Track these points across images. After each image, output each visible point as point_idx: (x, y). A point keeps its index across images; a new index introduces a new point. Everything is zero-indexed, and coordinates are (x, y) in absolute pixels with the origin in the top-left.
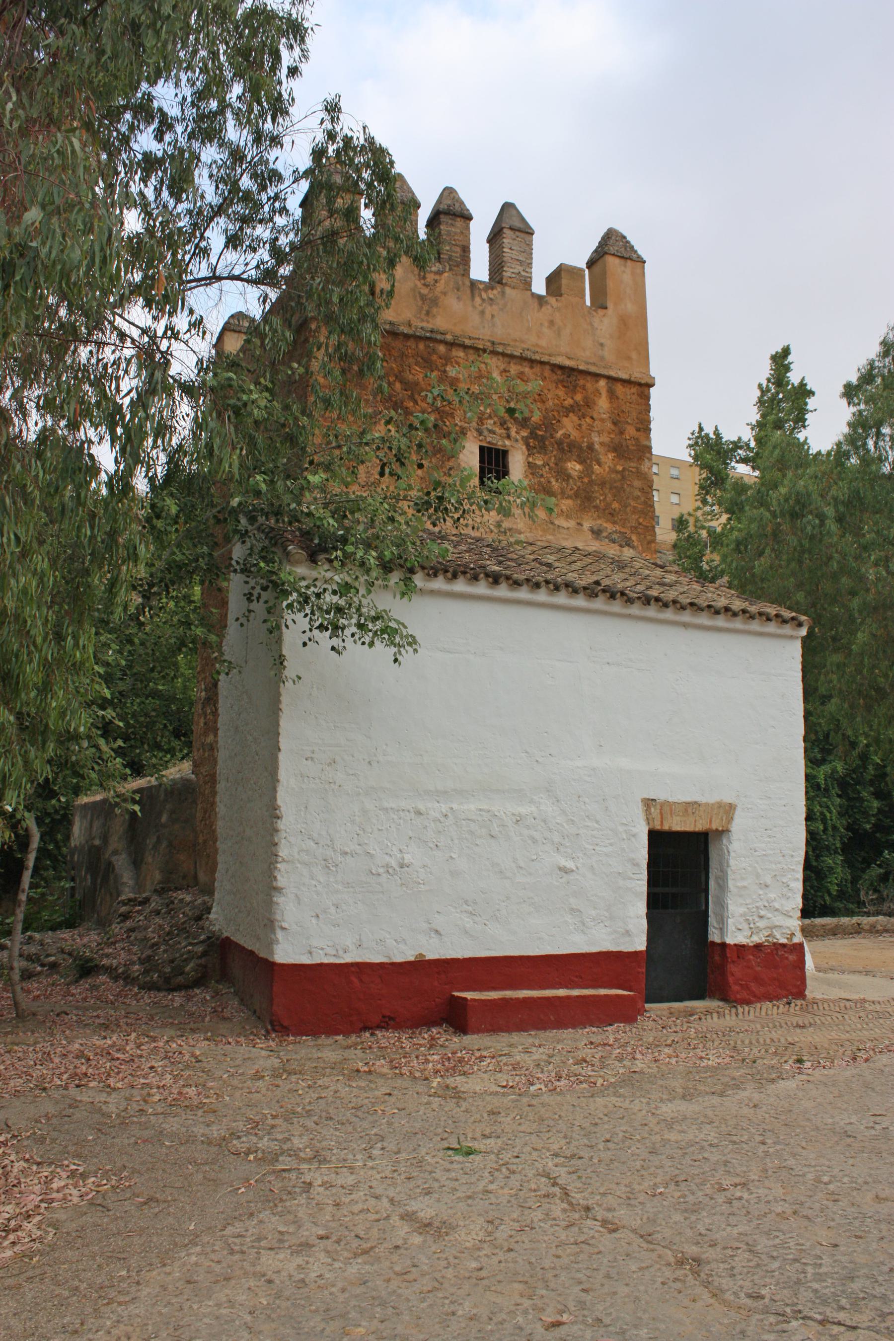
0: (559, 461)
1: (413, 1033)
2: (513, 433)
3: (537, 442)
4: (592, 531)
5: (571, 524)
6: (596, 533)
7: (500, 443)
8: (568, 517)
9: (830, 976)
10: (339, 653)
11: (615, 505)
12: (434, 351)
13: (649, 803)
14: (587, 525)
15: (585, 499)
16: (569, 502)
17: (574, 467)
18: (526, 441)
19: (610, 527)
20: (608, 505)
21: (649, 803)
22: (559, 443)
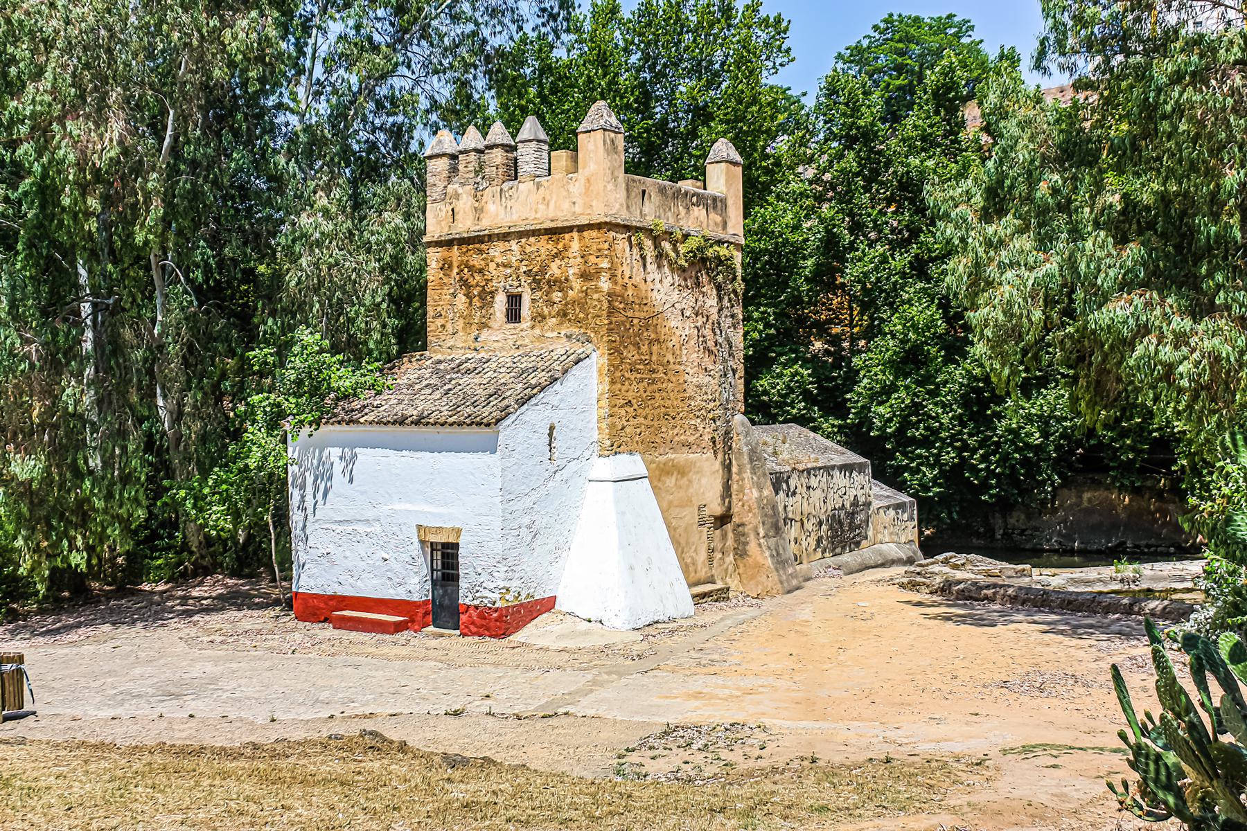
6: (569, 337)
13: (419, 527)
21: (419, 527)
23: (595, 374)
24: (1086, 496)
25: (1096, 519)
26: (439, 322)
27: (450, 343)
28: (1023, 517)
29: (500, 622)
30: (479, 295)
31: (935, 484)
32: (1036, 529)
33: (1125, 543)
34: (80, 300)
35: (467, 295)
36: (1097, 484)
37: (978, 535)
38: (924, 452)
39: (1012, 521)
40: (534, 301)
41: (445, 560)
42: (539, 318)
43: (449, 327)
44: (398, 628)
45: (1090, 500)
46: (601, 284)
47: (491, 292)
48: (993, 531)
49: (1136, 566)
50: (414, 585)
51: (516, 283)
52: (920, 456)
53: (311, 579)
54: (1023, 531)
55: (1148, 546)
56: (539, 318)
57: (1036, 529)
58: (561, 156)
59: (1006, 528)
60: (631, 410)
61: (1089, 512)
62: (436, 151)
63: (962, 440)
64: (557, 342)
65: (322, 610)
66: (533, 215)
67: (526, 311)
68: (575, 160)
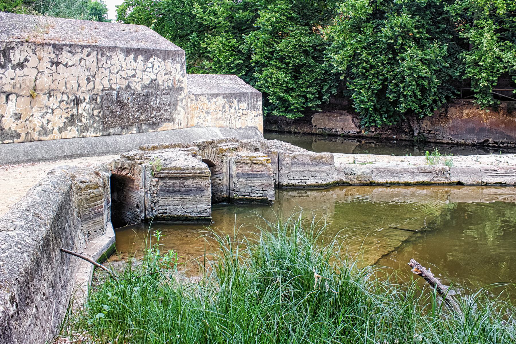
24: (465, 112)
25: (471, 125)
28: (429, 123)
31: (369, 100)
32: (436, 130)
33: (488, 140)
36: (471, 105)
37: (406, 133)
38: (362, 82)
39: (423, 125)
44: (390, 147)
45: (467, 114)
48: (412, 131)
49: (447, 157)
52: (361, 85)
54: (430, 131)
55: (502, 143)
57: (436, 130)
59: (420, 129)
61: (467, 121)
63: (383, 75)
66: (22, 168)
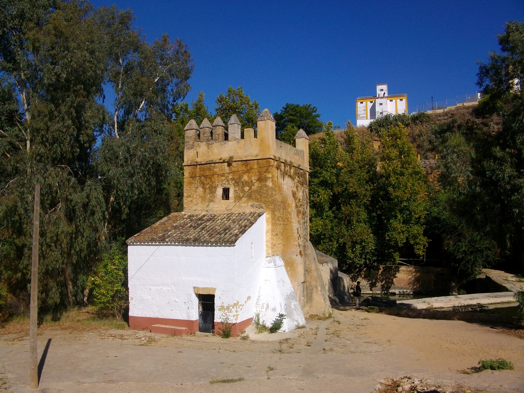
0: (243, 188)
1: (145, 50)
2: (230, 183)
3: (237, 183)
4: (251, 206)
5: (246, 205)
6: (252, 206)
7: (227, 186)
8: (245, 203)
9: (305, 289)
10: (269, 367)
11: (258, 197)
12: (211, 166)
13: (194, 288)
14: (250, 204)
15: (250, 197)
16: (245, 199)
17: (247, 188)
18: (234, 184)
19: (256, 204)
20: (256, 197)
21: (194, 288)
22: (243, 182)
23: (265, 222)
26: (189, 199)
27: (195, 208)
29: (227, 331)
30: (209, 187)
34: (113, 202)
35: (203, 188)
40: (235, 191)
41: (207, 301)
42: (238, 198)
43: (194, 201)
46: (268, 184)
47: (215, 187)
50: (193, 312)
51: (227, 183)
53: (136, 310)
56: (238, 198)
58: (249, 132)
60: (277, 237)
62: (190, 128)
64: (246, 208)
65: (148, 324)
67: (231, 194)
68: (255, 133)
